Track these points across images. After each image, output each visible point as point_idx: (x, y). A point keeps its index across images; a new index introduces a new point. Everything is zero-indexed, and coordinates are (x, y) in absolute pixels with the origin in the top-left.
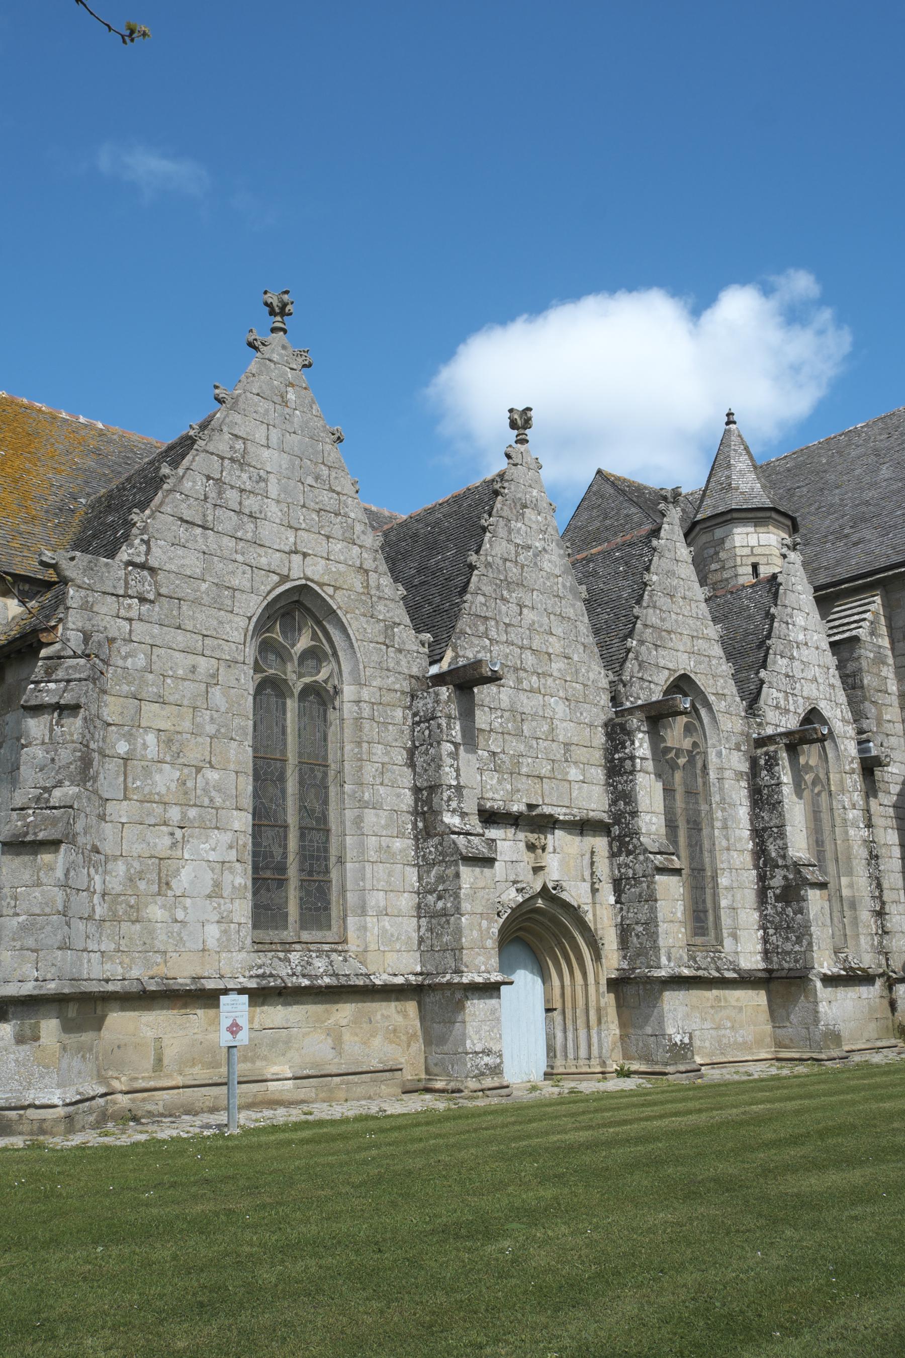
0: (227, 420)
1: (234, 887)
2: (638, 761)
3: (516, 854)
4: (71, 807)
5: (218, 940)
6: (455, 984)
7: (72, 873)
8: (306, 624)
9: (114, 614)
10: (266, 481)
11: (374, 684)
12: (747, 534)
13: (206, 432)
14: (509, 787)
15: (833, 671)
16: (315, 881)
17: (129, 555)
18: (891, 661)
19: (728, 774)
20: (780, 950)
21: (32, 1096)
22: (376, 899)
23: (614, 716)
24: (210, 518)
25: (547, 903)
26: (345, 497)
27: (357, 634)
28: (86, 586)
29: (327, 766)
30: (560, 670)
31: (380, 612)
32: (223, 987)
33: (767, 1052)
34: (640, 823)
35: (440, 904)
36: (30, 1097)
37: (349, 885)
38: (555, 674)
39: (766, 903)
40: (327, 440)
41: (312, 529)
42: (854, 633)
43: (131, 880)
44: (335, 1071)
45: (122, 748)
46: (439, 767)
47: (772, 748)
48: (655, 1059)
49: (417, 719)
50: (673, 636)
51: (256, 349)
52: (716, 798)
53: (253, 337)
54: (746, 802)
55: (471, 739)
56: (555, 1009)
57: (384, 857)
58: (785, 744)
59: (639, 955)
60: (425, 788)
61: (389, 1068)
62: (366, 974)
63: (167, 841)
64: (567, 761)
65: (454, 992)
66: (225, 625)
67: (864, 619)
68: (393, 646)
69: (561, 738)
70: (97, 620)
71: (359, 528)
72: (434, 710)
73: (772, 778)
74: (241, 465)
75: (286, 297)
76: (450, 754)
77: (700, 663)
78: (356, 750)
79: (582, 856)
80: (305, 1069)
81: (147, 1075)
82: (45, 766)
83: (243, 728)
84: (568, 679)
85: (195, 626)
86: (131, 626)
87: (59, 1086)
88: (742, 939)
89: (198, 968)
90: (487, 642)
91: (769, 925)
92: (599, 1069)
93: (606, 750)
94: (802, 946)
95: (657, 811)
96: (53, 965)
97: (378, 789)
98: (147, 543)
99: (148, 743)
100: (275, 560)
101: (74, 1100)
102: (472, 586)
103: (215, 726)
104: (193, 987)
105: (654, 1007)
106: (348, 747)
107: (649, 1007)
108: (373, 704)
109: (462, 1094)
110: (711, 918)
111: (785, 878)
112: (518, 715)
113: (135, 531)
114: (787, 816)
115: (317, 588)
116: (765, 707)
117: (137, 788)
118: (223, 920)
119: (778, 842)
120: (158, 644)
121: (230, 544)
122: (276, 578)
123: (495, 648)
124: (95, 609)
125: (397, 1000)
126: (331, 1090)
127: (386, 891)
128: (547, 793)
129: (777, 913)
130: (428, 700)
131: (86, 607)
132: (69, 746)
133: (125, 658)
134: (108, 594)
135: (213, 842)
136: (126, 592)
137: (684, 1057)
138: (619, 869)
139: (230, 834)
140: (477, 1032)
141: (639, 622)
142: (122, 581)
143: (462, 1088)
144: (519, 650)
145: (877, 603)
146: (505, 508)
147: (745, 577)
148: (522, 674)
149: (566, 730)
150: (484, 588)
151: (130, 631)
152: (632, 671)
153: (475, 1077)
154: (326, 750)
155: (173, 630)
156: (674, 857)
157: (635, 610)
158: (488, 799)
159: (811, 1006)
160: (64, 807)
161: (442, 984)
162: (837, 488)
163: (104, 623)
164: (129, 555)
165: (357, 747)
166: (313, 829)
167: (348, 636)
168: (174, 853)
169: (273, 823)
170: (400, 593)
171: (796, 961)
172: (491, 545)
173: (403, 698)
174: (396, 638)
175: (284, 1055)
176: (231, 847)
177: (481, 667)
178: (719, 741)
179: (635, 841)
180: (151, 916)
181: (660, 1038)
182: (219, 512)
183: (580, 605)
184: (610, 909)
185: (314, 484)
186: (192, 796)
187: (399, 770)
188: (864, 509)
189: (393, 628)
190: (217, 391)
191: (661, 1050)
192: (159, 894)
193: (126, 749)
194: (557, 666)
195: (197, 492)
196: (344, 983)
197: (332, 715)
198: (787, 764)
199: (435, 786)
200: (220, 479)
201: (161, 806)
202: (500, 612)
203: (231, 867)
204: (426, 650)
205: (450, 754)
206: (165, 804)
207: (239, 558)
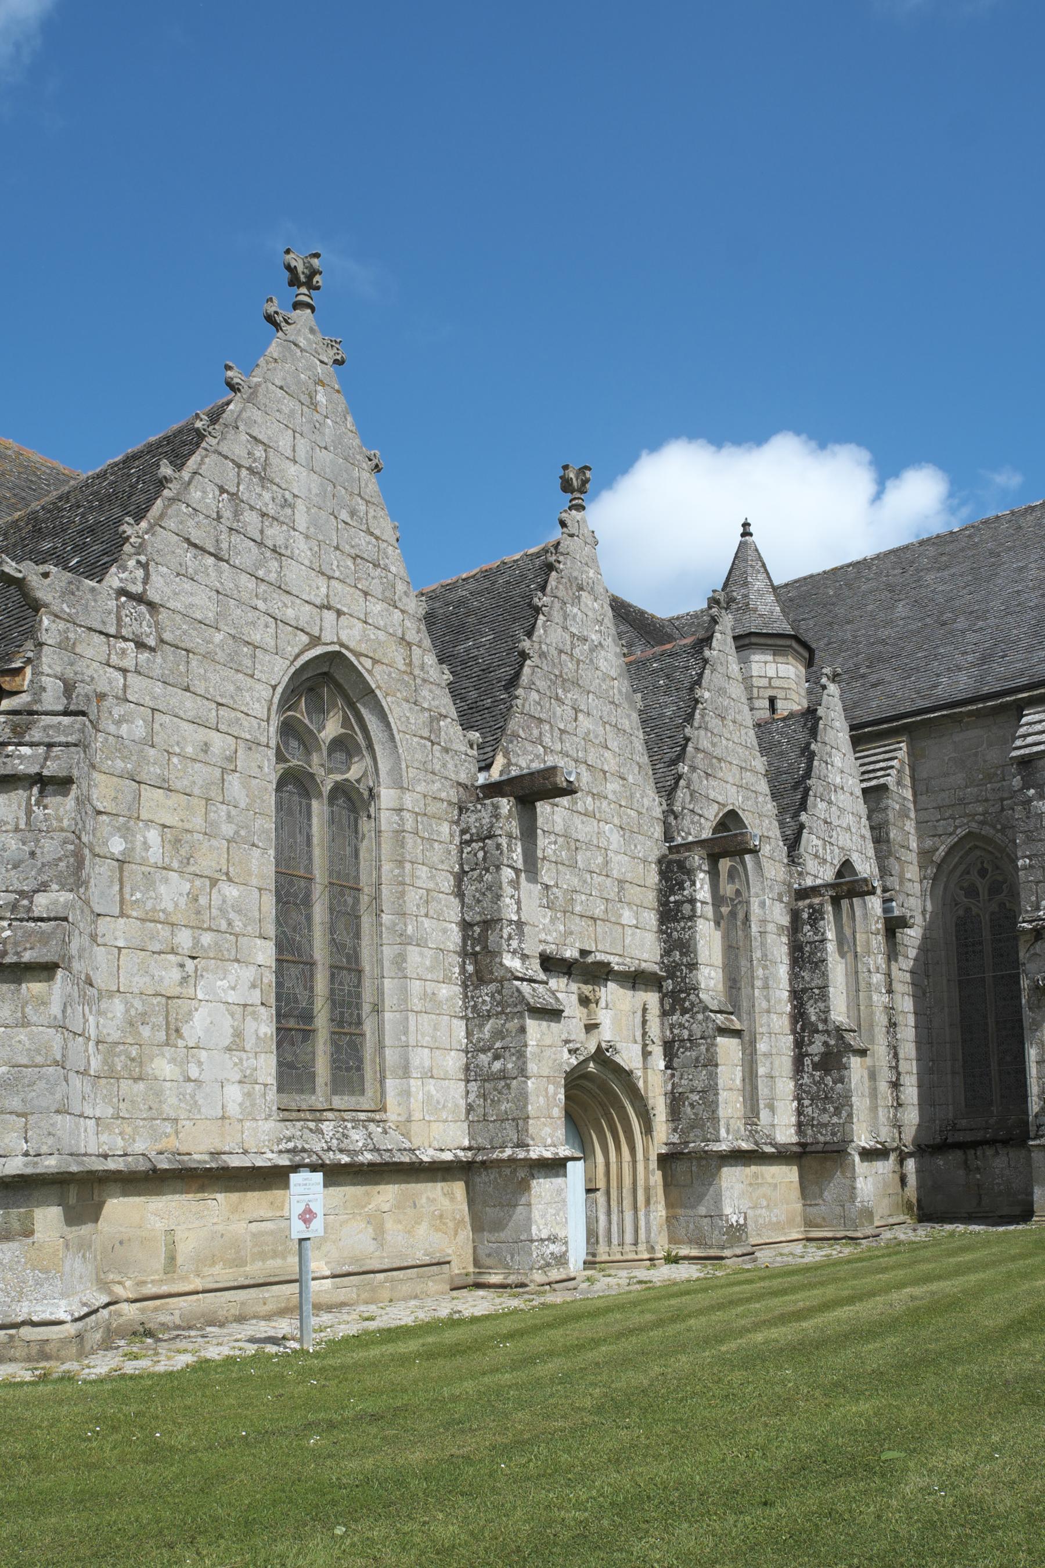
0: (244, 415)
1: (258, 1037)
2: (699, 904)
4: (65, 919)
5: (240, 1105)
6: (521, 1160)
7: (69, 1010)
8: (335, 705)
9: (103, 659)
10: (292, 507)
11: (418, 789)
12: (766, 663)
13: (216, 427)
14: (562, 928)
15: (864, 821)
16: (345, 1034)
17: (121, 580)
18: (912, 815)
19: (771, 927)
20: (815, 1123)
21: (25, 1310)
22: (420, 1058)
23: (667, 852)
24: (224, 545)
25: (599, 1067)
26: (385, 545)
27: (399, 723)
28: (65, 616)
29: (359, 890)
30: (614, 792)
31: (424, 698)
32: (250, 1165)
33: (798, 1232)
34: (699, 977)
35: (497, 1065)
36: (22, 1311)
37: (388, 1041)
38: (610, 796)
39: (803, 1071)
40: (364, 465)
41: (348, 581)
42: (882, 781)
43: (131, 1024)
44: (378, 1266)
45: (117, 846)
46: (499, 897)
47: (816, 901)
48: (709, 1243)
49: (467, 837)
50: (723, 764)
51: (277, 326)
52: (757, 954)
53: (274, 309)
54: (786, 960)
55: (531, 866)
56: (598, 1190)
57: (429, 1005)
58: (831, 897)
59: (693, 1127)
60: (478, 923)
62: (410, 1150)
63: (176, 974)
64: (621, 901)
65: (515, 1170)
66: (245, 694)
67: (892, 767)
68: (439, 744)
70: (81, 665)
71: (401, 587)
72: (492, 827)
73: (816, 934)
74: (262, 479)
75: (315, 262)
77: (748, 799)
78: (396, 872)
80: (344, 1265)
81: (157, 1277)
82: (21, 861)
83: (266, 831)
84: (623, 804)
85: (207, 690)
86: (125, 680)
87: (63, 1295)
88: (779, 1111)
89: (217, 1140)
90: (542, 750)
91: (804, 1095)
92: (646, 1256)
93: (660, 891)
94: (840, 1118)
95: (716, 964)
96: (50, 1134)
97: (422, 922)
98: (145, 566)
99: (150, 842)
100: (304, 614)
101: (82, 1313)
102: (524, 679)
103: (233, 826)
104: (214, 1165)
105: (710, 1184)
106: (386, 867)
107: (703, 1184)
108: (417, 814)
109: (527, 1289)
111: (826, 1044)
112: (574, 844)
113: (127, 548)
114: (831, 976)
115: (353, 659)
116: (806, 854)
117: (137, 901)
118: (246, 1080)
119: (820, 1004)
120: (161, 708)
121: (250, 585)
122: (305, 639)
124: (78, 650)
125: (444, 1180)
126: (373, 1290)
127: (432, 1049)
128: (600, 937)
129: (815, 1083)
130: (483, 814)
131: (66, 646)
132: (55, 835)
133: (118, 723)
134: (95, 631)
135: (232, 978)
136: (117, 631)
137: (739, 1239)
138: (671, 1029)
139: (253, 969)
140: (543, 1216)
141: (690, 744)
142: (113, 616)
143: (527, 1281)
145: (902, 750)
146: (561, 586)
147: (762, 712)
149: (620, 865)
150: (538, 683)
151: (125, 685)
152: (683, 801)
153: (540, 1268)
154: (358, 870)
155: (179, 691)
156: (733, 1017)
157: (686, 730)
159: (848, 1182)
160: (56, 919)
161: (502, 1161)
162: (848, 623)
163: (89, 672)
164: (121, 580)
165: (397, 868)
167: (388, 725)
168: (184, 991)
169: (297, 959)
170: (445, 677)
171: (834, 1134)
172: (545, 631)
173: (450, 810)
174: (443, 733)
175: (319, 1248)
176: (254, 986)
177: (556, 775)
178: (763, 889)
179: (692, 997)
180: (157, 1072)
181: (716, 1220)
182: (235, 539)
183: (635, 716)
184: (660, 1075)
185: (349, 520)
186: (206, 918)
187: (446, 900)
188: (880, 648)
190: (230, 373)
191: (717, 1232)
192: (167, 1044)
193: (122, 848)
194: (612, 787)
195: (207, 506)
196: (388, 1159)
197: (365, 826)
198: (831, 918)
199: (492, 920)
200: (236, 494)
201: (167, 928)
202: (554, 713)
203: (254, 1012)
204: (475, 753)
206: (173, 925)
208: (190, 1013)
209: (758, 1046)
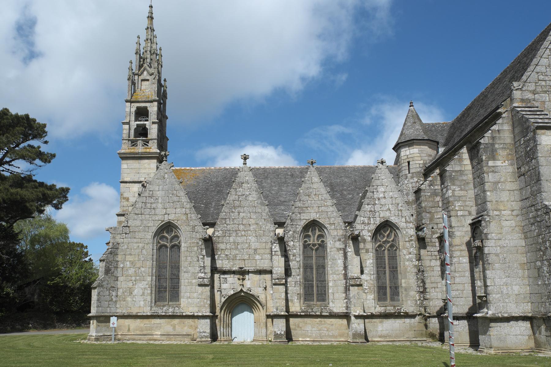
11: (188, 242)
12: (406, 151)
24: (143, 212)
30: (253, 228)
43: (123, 293)
44: (172, 334)
45: (122, 266)
63: (132, 284)
64: (255, 254)
69: (253, 248)
71: (185, 204)
76: (201, 258)
79: (260, 280)
84: (257, 230)
100: (160, 217)
110: (327, 296)
123: (229, 226)
135: (142, 284)
148: (238, 232)
174: (196, 229)
176: (147, 285)
189: (195, 227)
202: (231, 216)
207: (150, 219)
208: (134, 290)
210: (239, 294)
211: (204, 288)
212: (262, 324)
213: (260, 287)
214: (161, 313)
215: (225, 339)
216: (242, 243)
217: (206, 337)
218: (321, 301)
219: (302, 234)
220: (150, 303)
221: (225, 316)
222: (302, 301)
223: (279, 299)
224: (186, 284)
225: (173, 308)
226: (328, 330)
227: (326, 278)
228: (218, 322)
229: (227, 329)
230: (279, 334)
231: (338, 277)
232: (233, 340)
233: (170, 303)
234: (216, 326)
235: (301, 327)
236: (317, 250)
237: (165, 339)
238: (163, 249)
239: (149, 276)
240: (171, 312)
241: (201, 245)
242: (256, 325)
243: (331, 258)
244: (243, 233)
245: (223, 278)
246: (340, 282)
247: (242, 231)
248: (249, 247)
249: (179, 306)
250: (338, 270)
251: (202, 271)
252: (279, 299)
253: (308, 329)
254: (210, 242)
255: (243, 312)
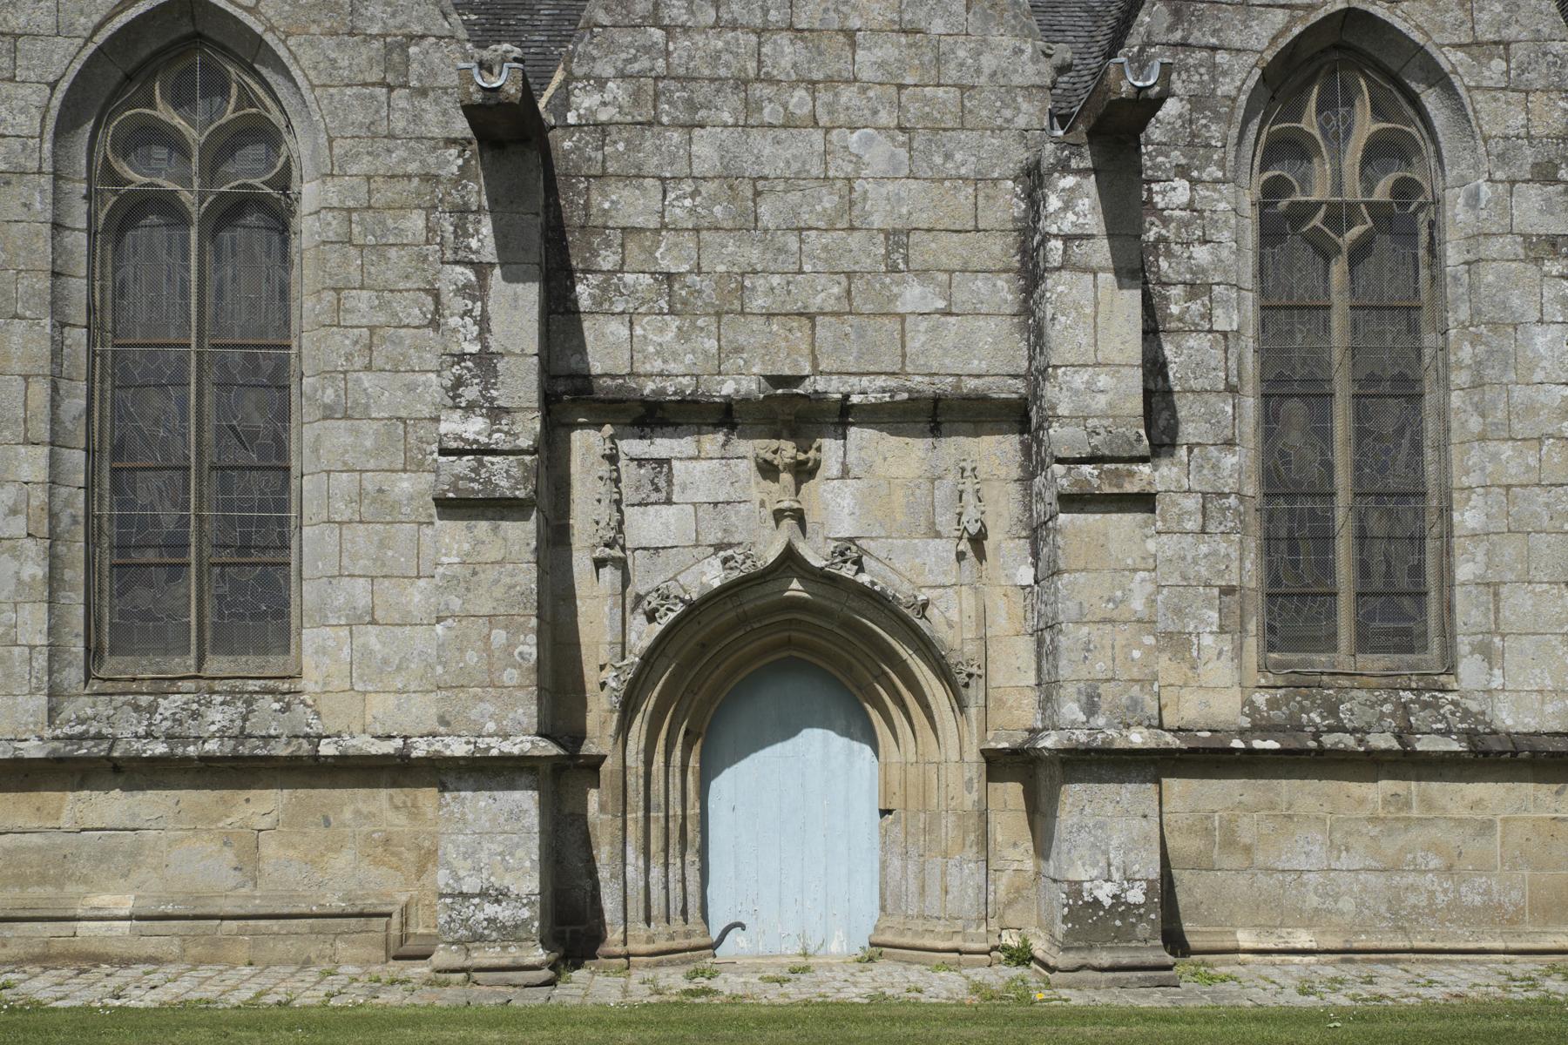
1: (19, 581)
3: (727, 486)
11: (354, 169)
16: (256, 564)
27: (312, 74)
30: (882, 65)
38: (865, 75)
44: (229, 909)
61: (356, 910)
68: (405, 86)
69: (877, 221)
76: (463, 290)
79: (932, 481)
84: (909, 80)
97: (358, 380)
108: (350, 210)
125: (394, 784)
127: (373, 578)
144: (754, 38)
158: (649, 375)
166: (251, 468)
169: (161, 463)
174: (415, 66)
176: (14, 512)
189: (404, 48)
203: (14, 548)
205: (463, 290)
209: (1456, 516)
210: (770, 587)
211: (483, 526)
212: (949, 821)
213: (938, 535)
214: (137, 745)
215: (662, 944)
216: (791, 182)
217: (510, 933)
218: (1385, 649)
219: (1253, 127)
220: (41, 661)
221: (659, 759)
222: (1252, 644)
223: (1112, 621)
224: (343, 511)
225: (241, 707)
226: (1450, 868)
227: (1431, 469)
228: (602, 808)
229: (675, 861)
230: (1107, 902)
231: (1532, 461)
232: (714, 946)
233: (215, 665)
234: (586, 843)
235: (1247, 849)
236: (1360, 252)
237: (176, 950)
238: (150, 233)
239: (28, 442)
240: (222, 734)
241: (456, 182)
242: (897, 832)
243: (1476, 312)
244: (799, 99)
245: (640, 462)
246: (1542, 497)
247: (793, 85)
248: (849, 217)
249: (285, 687)
250: (1531, 409)
251: (471, 393)
252: (1112, 621)
253: (1300, 862)
254: (534, 158)
255: (789, 731)
